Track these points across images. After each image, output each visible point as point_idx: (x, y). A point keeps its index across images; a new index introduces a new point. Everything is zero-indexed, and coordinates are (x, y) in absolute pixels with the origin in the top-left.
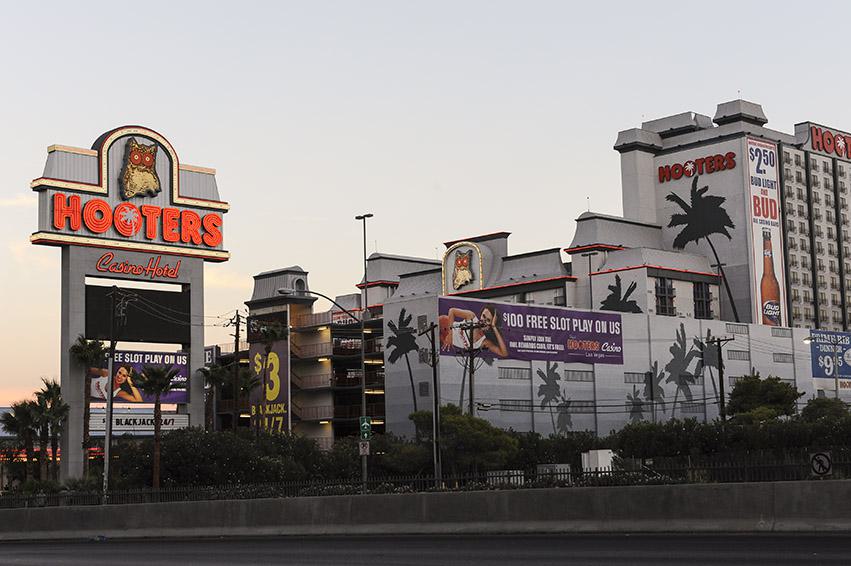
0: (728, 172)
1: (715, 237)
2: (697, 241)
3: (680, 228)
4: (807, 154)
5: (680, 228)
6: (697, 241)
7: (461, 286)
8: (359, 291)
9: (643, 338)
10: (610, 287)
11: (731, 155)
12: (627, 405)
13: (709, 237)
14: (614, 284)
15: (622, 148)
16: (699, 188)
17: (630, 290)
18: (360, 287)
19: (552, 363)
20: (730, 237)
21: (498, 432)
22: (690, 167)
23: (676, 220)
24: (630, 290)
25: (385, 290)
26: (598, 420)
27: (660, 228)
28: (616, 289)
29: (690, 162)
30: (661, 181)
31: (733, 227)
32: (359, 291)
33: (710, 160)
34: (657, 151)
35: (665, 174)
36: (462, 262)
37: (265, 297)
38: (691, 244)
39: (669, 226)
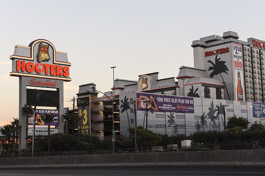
0: (227, 53)
1: (223, 74)
2: (217, 75)
3: (212, 71)
4: (251, 48)
5: (212, 71)
6: (217, 75)
7: (144, 89)
8: (112, 91)
9: (200, 105)
10: (190, 89)
11: (228, 48)
12: (195, 126)
13: (221, 74)
14: (191, 88)
15: (194, 46)
16: (218, 58)
17: (196, 90)
18: (112, 89)
19: (172, 113)
20: (227, 74)
21: (155, 134)
22: (215, 52)
23: (210, 68)
24: (196, 90)
25: (120, 90)
26: (186, 131)
27: (206, 71)
28: (192, 90)
29: (215, 50)
30: (206, 56)
31: (228, 70)
32: (112, 91)
33: (221, 50)
34: (205, 47)
35: (207, 54)
36: (144, 82)
37: (82, 92)
38: (215, 76)
39: (208, 70)
